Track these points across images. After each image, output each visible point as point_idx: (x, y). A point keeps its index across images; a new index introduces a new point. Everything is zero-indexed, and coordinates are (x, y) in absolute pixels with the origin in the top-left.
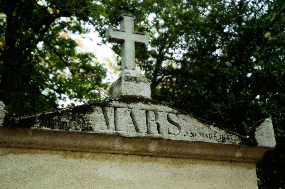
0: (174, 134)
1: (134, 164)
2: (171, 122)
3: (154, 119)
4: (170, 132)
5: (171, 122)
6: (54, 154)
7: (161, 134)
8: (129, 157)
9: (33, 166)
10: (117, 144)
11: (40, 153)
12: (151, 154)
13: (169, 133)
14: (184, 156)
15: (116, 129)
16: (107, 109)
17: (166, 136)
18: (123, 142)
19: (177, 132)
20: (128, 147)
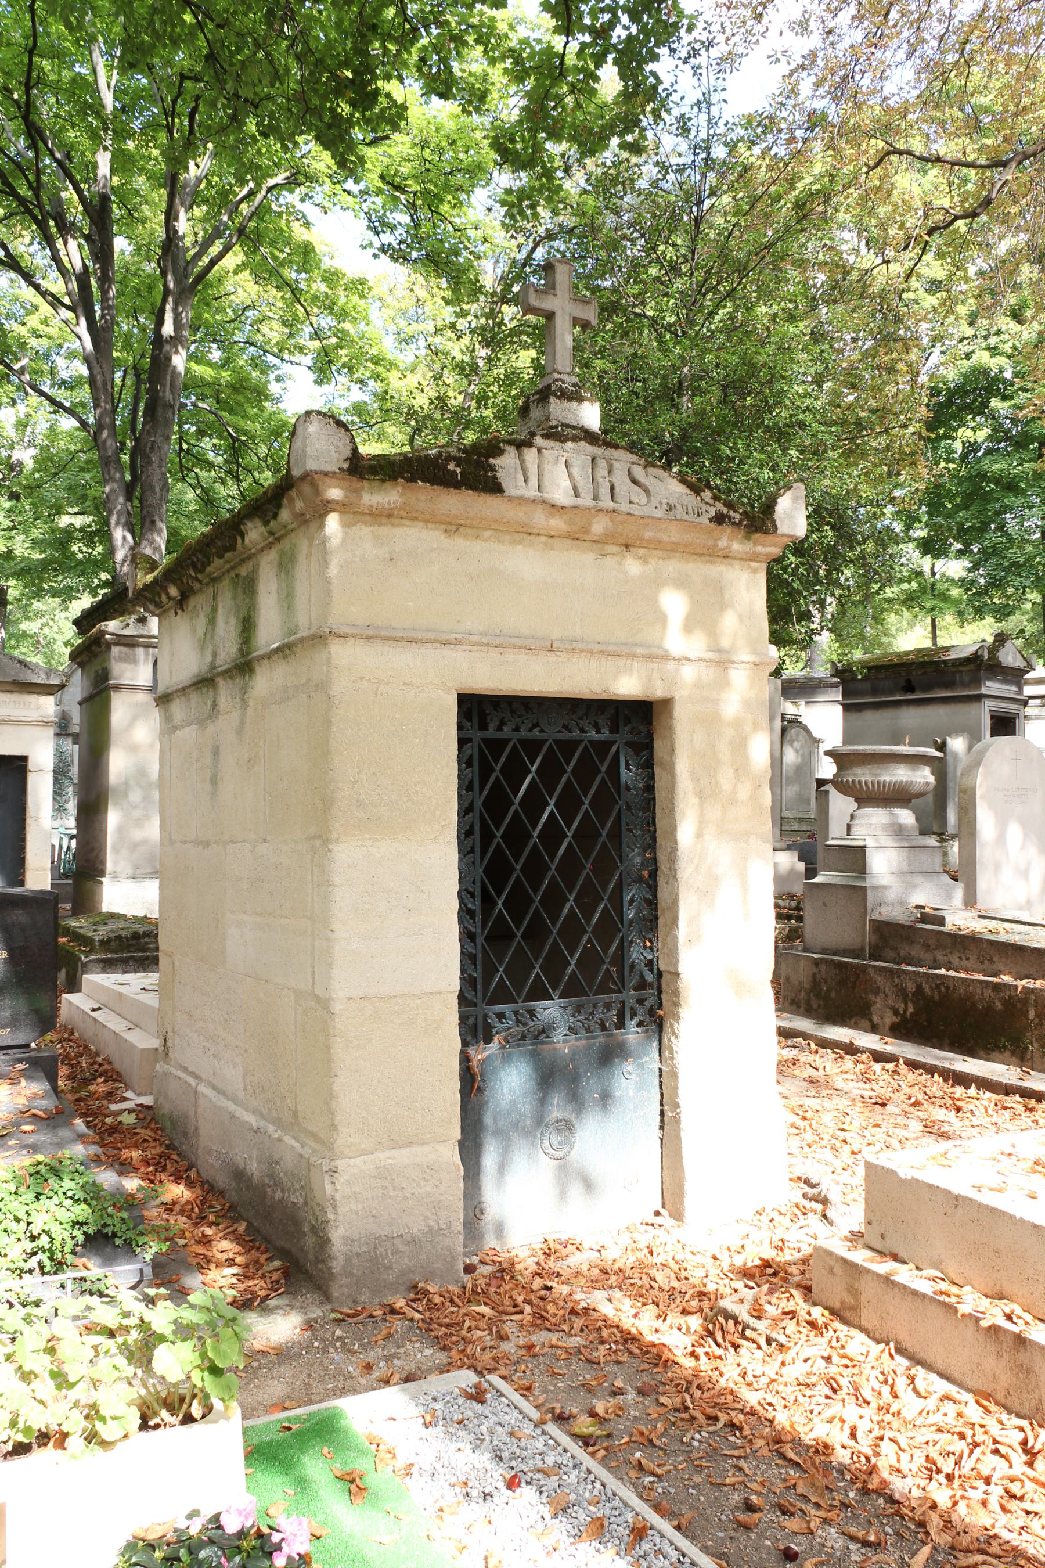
2: (635, 482)
5: (635, 482)
8: (556, 541)
10: (540, 519)
13: (631, 502)
16: (526, 450)
17: (624, 507)
19: (644, 500)
20: (557, 523)
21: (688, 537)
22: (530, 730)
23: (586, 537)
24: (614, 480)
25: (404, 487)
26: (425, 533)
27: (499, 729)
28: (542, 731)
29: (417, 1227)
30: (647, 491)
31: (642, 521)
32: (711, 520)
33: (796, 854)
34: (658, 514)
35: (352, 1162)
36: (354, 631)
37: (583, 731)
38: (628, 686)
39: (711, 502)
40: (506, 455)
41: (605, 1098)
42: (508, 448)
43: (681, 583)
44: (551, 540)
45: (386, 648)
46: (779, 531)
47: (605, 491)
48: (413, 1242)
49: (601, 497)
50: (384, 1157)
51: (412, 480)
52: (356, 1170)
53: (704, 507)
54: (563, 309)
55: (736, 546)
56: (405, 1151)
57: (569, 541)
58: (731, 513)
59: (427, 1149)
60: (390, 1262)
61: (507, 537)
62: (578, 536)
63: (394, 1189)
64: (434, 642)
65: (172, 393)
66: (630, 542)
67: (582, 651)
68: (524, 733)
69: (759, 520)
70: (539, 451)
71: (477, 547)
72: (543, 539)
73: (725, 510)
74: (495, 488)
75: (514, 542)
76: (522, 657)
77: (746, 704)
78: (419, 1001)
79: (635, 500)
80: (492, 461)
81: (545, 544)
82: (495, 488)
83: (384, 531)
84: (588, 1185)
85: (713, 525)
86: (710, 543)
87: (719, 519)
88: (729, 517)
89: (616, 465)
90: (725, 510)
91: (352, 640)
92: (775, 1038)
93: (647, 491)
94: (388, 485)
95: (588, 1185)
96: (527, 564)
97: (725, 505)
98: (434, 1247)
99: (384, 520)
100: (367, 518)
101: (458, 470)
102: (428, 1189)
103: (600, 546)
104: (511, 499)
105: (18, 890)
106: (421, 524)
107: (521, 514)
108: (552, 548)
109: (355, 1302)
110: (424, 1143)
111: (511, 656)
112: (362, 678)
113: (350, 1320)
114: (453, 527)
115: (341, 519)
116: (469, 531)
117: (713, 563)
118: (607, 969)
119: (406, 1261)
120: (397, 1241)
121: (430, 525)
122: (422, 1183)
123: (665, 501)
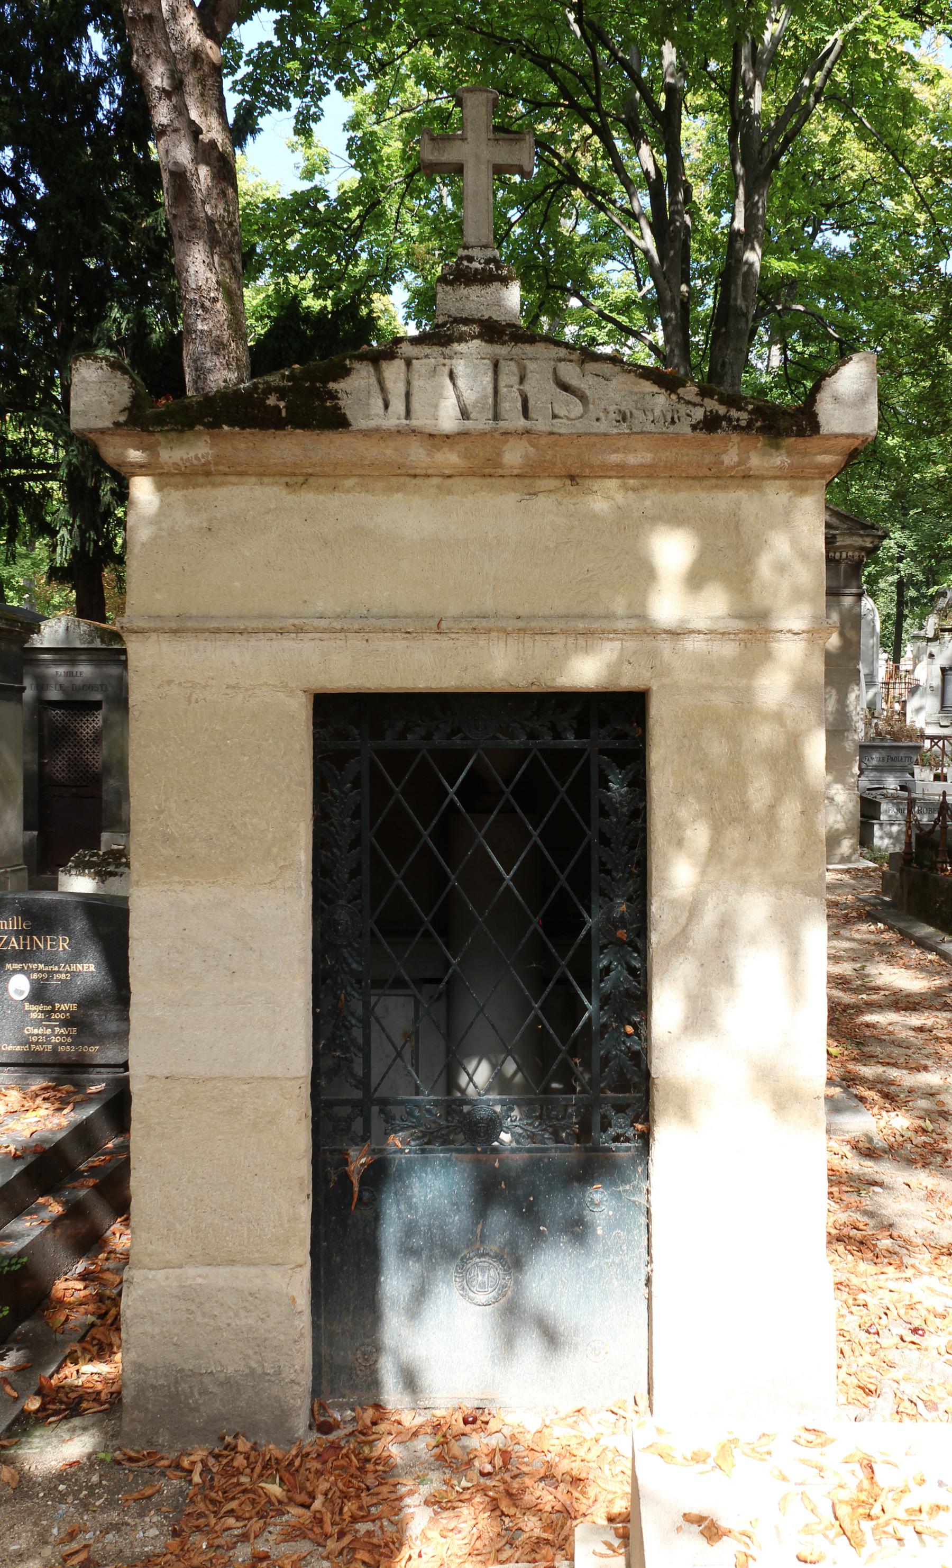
0: (568, 419)
1: (470, 497)
2: (565, 387)
3: (515, 379)
4: (556, 412)
5: (565, 387)
6: (268, 484)
7: (532, 419)
8: (457, 481)
9: (219, 516)
10: (418, 454)
11: (234, 484)
12: (516, 472)
13: (555, 416)
14: (608, 474)
15: (408, 414)
16: (384, 365)
17: (541, 424)
18: (434, 446)
19: (578, 409)
20: (451, 458)
21: (669, 455)
22: (449, 737)
23: (500, 472)
24: (526, 387)
25: (212, 436)
26: (258, 492)
27: (402, 736)
28: (465, 738)
29: (233, 1365)
30: (583, 398)
31: (583, 441)
32: (694, 427)
33: (98, 1028)
34: (602, 427)
35: (151, 1274)
36: (159, 624)
37: (532, 736)
38: (587, 670)
39: (697, 400)
40: (354, 375)
41: (578, 1229)
42: (357, 365)
43: (676, 519)
44: (450, 481)
45: (202, 643)
46: (824, 430)
47: (511, 405)
48: (227, 1383)
49: (504, 414)
50: (195, 1275)
51: (215, 425)
52: (153, 1286)
53: (683, 409)
54: (477, 157)
55: (756, 461)
56: (224, 1271)
57: (477, 480)
58: (734, 413)
59: (253, 1271)
60: (196, 1402)
61: (380, 484)
62: (487, 471)
63: (204, 1315)
64: (265, 631)
65: (745, 299)
66: (574, 471)
67: (489, 631)
68: (438, 740)
69: (788, 420)
70: (408, 363)
71: (332, 502)
72: (436, 481)
73: (722, 410)
74: (337, 421)
75: (390, 490)
76: (400, 644)
77: (801, 686)
78: (245, 1087)
79: (561, 411)
80: (332, 385)
81: (439, 488)
82: (337, 421)
83: (201, 494)
84: (551, 1337)
85: (701, 435)
86: (708, 459)
87: (710, 424)
88: (729, 419)
89: (531, 366)
90: (722, 410)
91: (154, 636)
92: (823, 1185)
93: (583, 398)
94: (188, 435)
95: (551, 1337)
96: (408, 517)
97: (721, 401)
98: (257, 1394)
99: (201, 479)
100: (179, 479)
101: (282, 404)
102: (251, 1321)
103: (527, 481)
104: (367, 434)
105: (47, 896)
106: (253, 479)
107: (389, 452)
108: (449, 492)
109: (150, 1443)
110: (251, 1264)
111: (382, 643)
112: (170, 682)
113: (127, 1465)
114: (298, 478)
115: (155, 482)
116: (322, 481)
117: (725, 488)
118: (564, 1061)
119: (218, 1404)
120: (206, 1379)
121: (266, 480)
122: (242, 1313)
123: (613, 408)
